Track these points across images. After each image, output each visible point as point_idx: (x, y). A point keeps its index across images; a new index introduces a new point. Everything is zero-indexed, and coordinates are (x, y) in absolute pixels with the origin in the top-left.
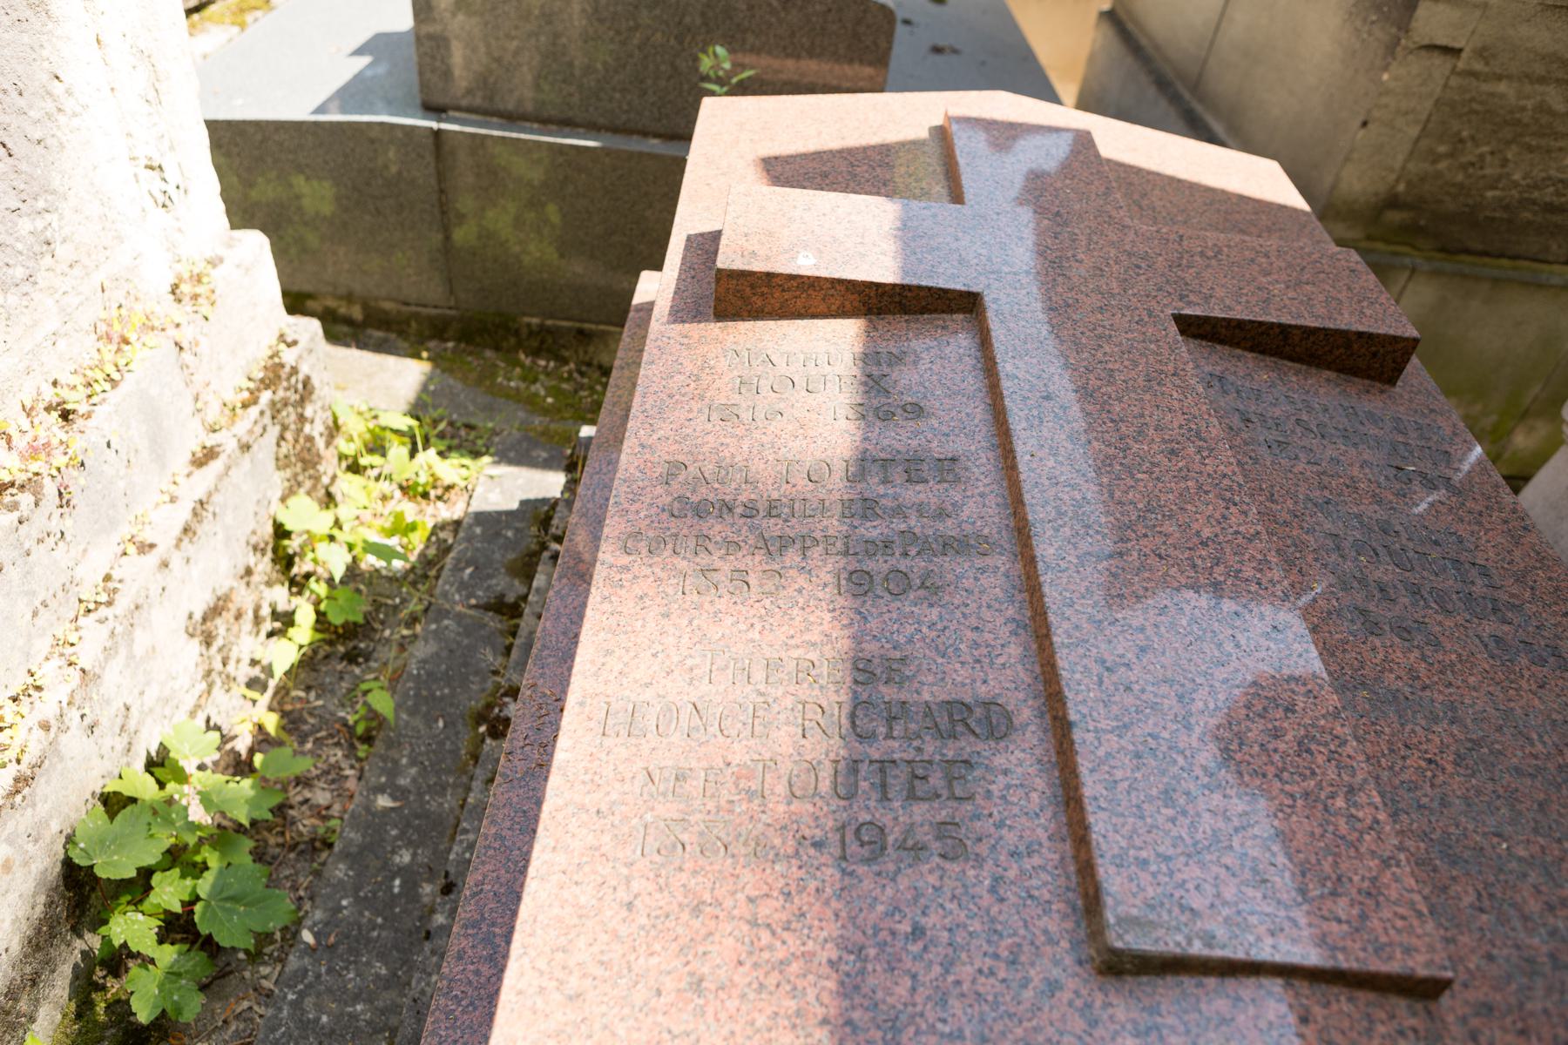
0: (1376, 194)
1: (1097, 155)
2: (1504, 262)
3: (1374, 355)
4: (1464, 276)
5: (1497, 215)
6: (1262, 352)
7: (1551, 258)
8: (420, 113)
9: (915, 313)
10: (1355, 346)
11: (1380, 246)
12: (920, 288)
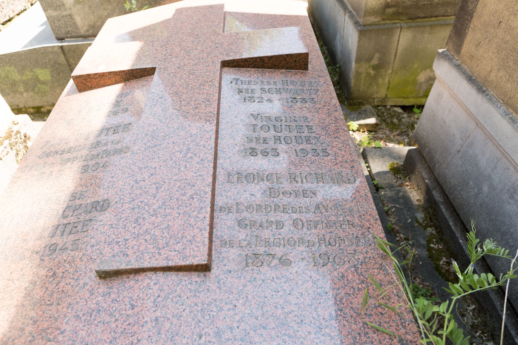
0: (381, 4)
1: (110, 15)
2: (433, 19)
3: (295, 61)
4: (419, 26)
5: (426, 3)
6: (258, 68)
7: (449, 14)
8: (56, 40)
9: (139, 78)
10: (288, 60)
11: (388, 22)
12: (136, 69)
